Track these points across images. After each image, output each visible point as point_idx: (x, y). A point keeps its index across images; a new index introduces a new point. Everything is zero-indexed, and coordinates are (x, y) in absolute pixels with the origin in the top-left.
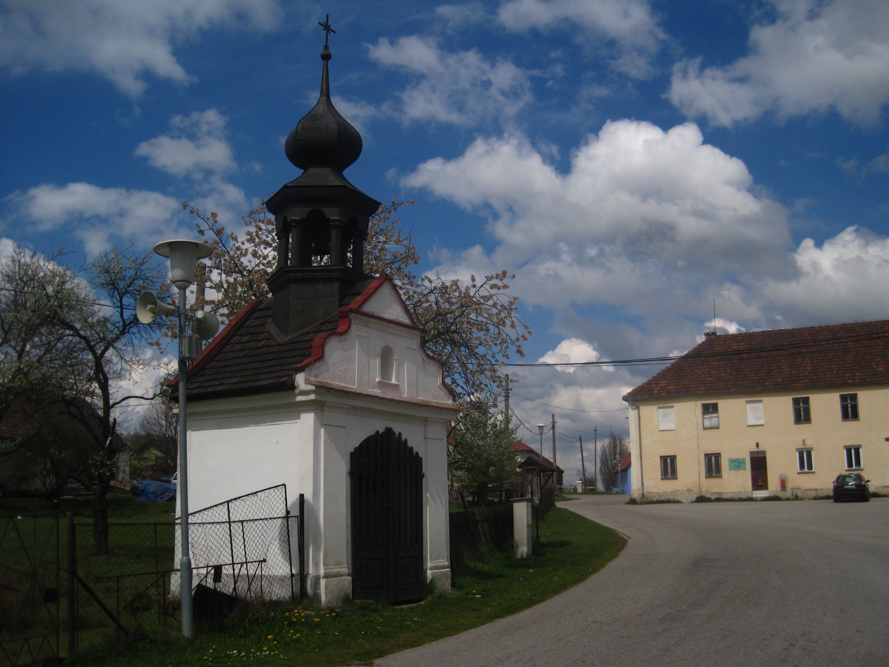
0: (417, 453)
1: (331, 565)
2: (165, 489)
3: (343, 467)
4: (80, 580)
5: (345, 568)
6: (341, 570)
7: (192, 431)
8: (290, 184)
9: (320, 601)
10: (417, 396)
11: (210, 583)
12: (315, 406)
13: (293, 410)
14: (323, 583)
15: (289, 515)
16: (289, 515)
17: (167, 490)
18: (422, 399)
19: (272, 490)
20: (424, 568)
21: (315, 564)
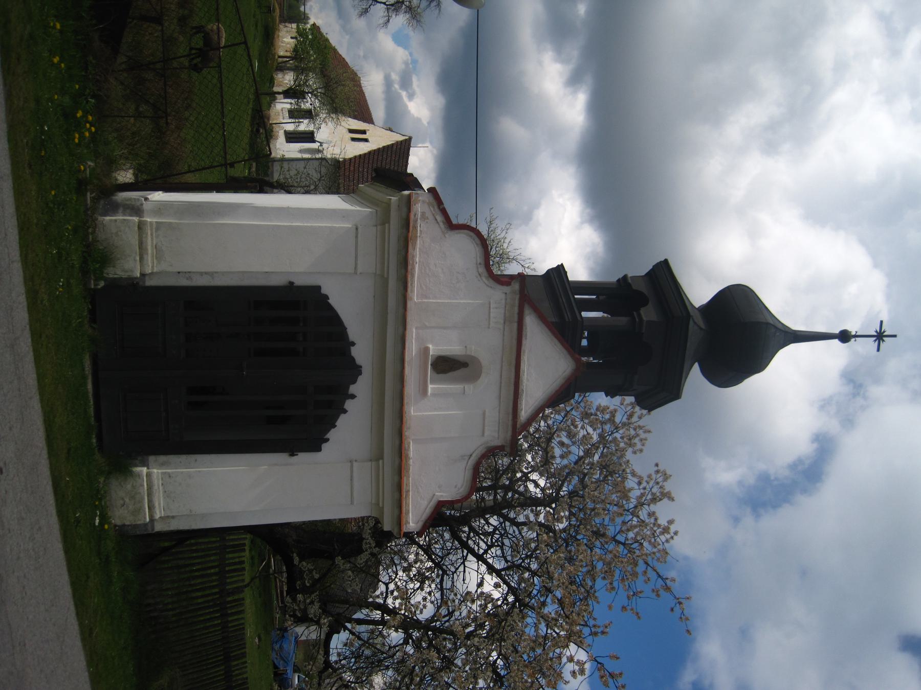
1: (157, 237)
2: (286, 660)
5: (153, 267)
9: (105, 214)
14: (136, 219)
15: (228, 166)
16: (228, 166)
17: (286, 662)
18: (411, 454)
20: (152, 459)
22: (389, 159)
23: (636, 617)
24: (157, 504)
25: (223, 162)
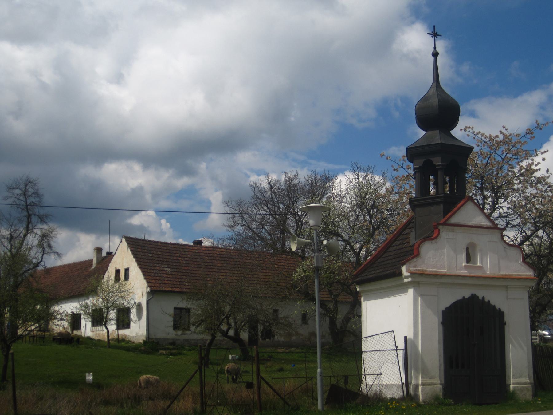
0: (500, 309)
3: (435, 322)
4: (262, 377)
5: (438, 380)
6: (435, 381)
7: (367, 301)
8: (411, 146)
10: (499, 271)
11: (342, 384)
12: (414, 284)
13: (402, 288)
14: (420, 388)
18: (504, 273)
19: (384, 334)
20: (507, 383)
21: (416, 377)
22: (142, 254)
23: (547, 153)
24: (524, 381)
25: (395, 351)
